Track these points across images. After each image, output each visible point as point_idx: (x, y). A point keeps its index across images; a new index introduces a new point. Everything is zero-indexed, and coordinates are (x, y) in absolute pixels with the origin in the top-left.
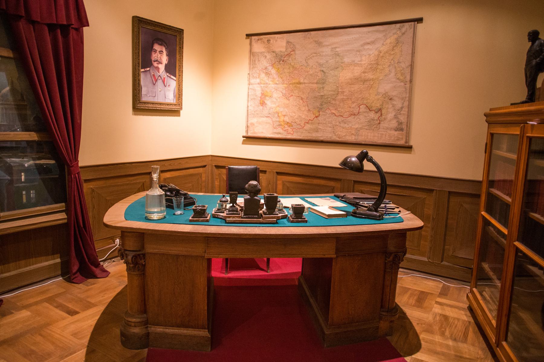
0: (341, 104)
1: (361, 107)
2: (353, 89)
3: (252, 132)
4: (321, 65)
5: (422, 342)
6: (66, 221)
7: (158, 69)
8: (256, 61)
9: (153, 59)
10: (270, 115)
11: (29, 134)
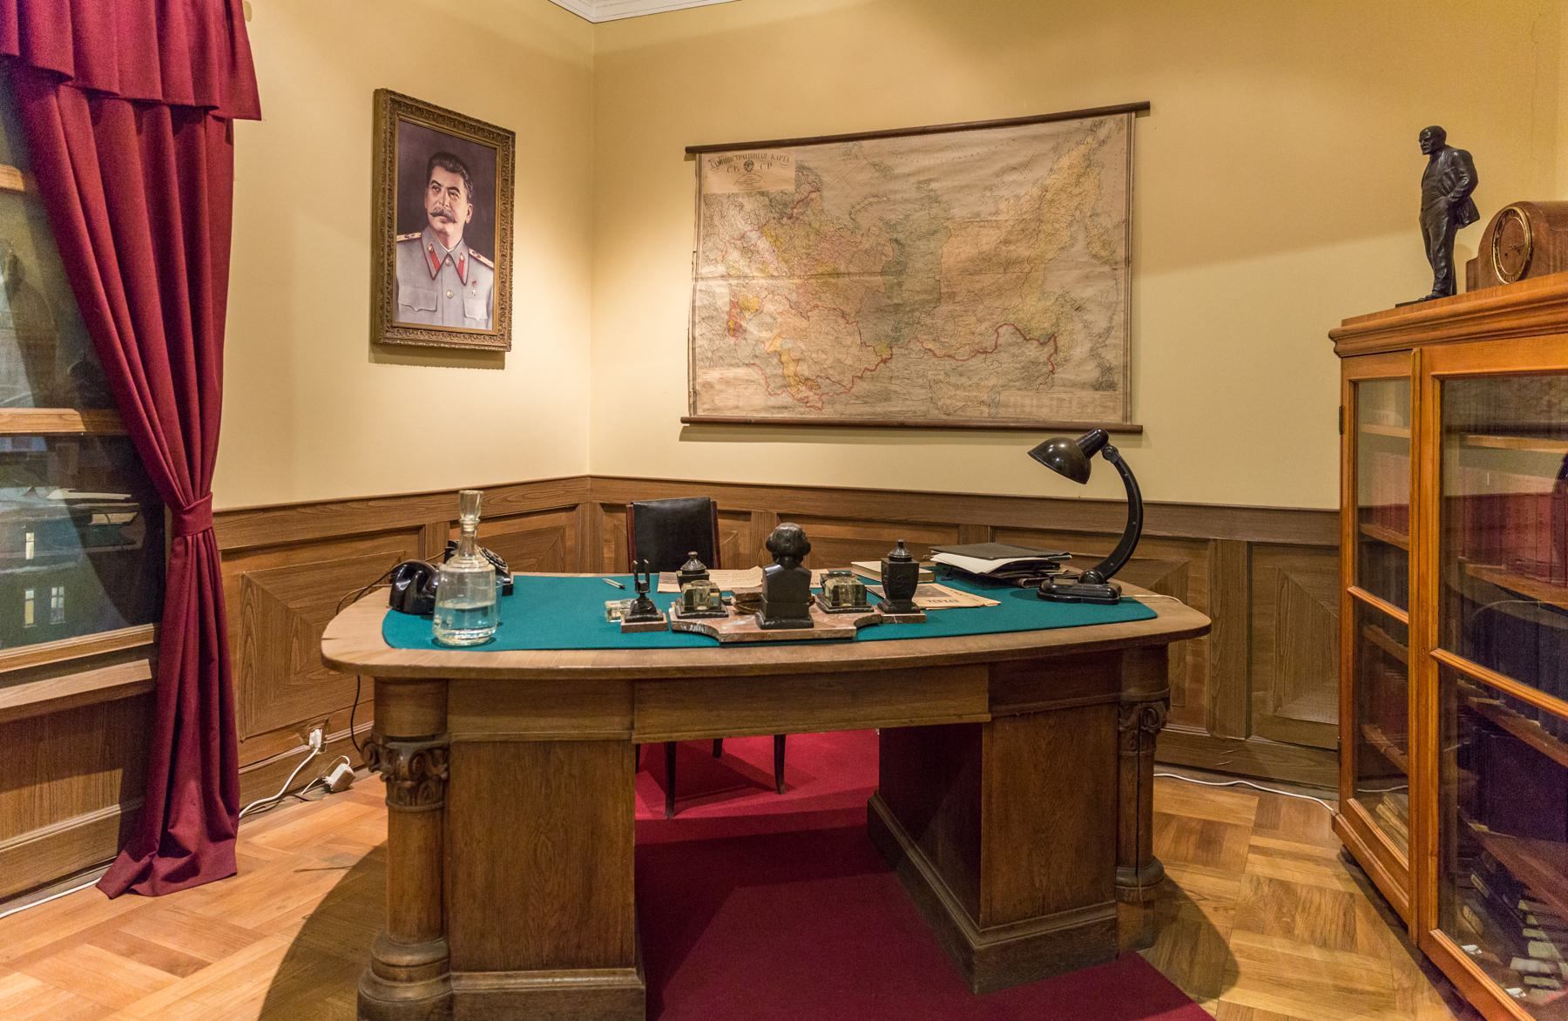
0: (950, 327)
2: (978, 286)
4: (891, 227)
5: (1238, 959)
7: (443, 235)
9: (430, 210)
10: (757, 361)
11: (60, 416)
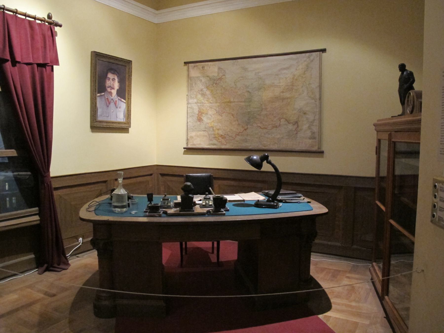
1: (282, 120)
3: (191, 144)
6: (38, 222)
7: (111, 93)
8: (194, 84)
9: (107, 85)
10: (206, 129)
